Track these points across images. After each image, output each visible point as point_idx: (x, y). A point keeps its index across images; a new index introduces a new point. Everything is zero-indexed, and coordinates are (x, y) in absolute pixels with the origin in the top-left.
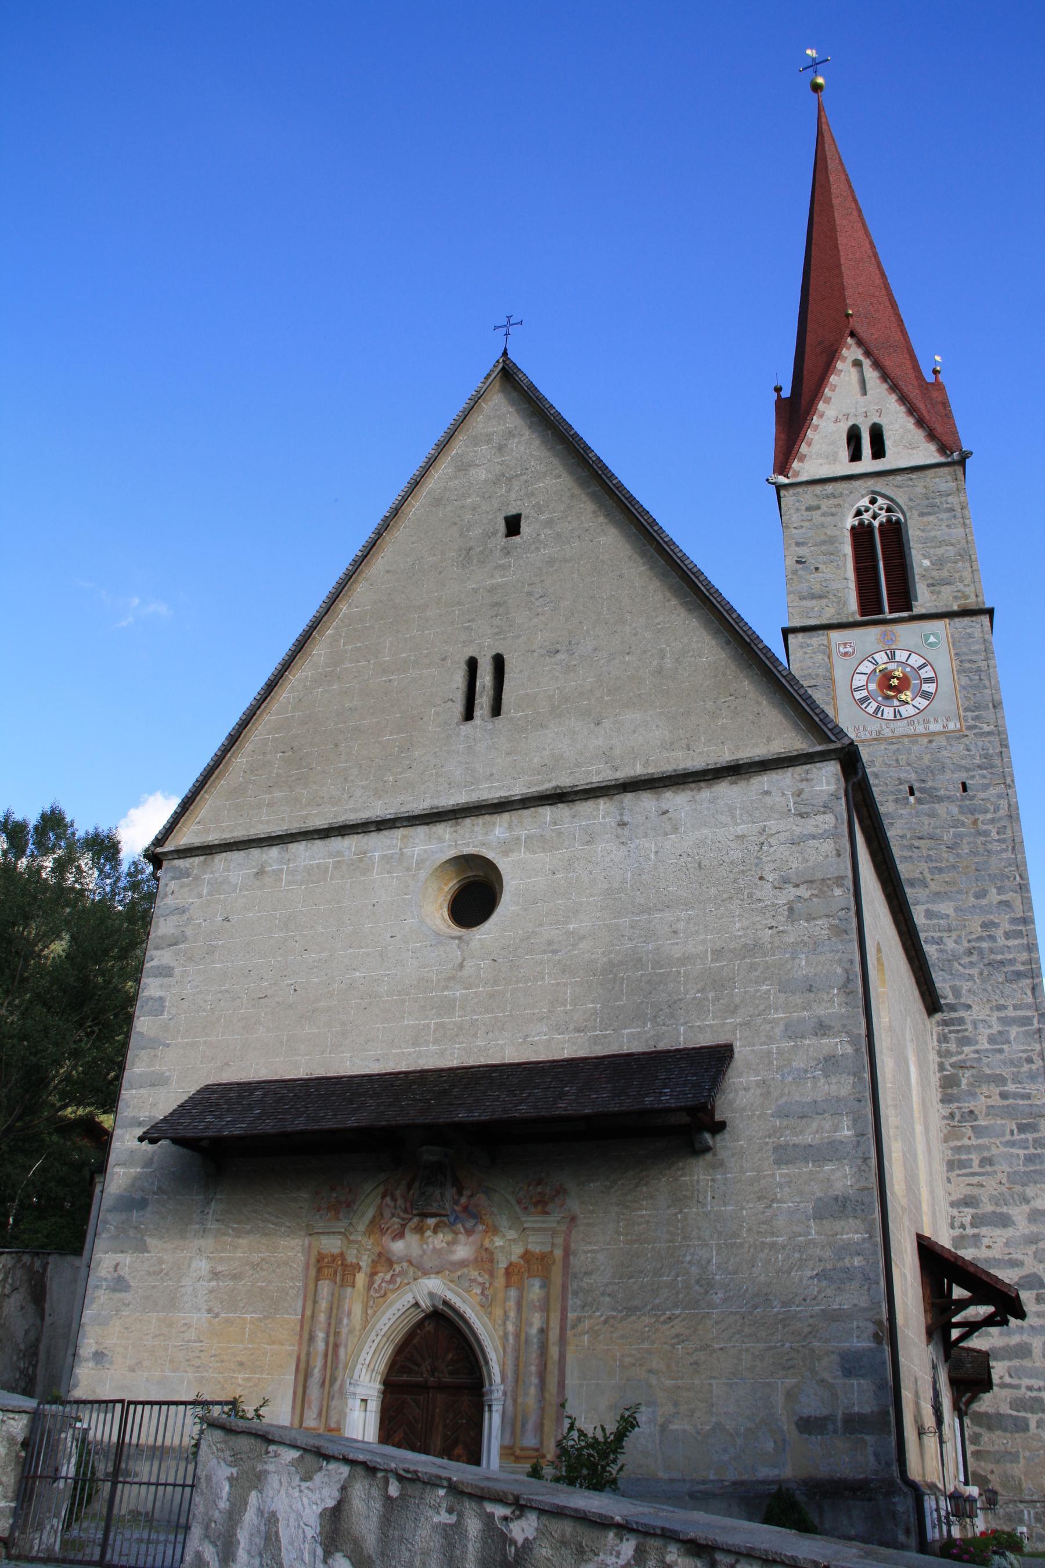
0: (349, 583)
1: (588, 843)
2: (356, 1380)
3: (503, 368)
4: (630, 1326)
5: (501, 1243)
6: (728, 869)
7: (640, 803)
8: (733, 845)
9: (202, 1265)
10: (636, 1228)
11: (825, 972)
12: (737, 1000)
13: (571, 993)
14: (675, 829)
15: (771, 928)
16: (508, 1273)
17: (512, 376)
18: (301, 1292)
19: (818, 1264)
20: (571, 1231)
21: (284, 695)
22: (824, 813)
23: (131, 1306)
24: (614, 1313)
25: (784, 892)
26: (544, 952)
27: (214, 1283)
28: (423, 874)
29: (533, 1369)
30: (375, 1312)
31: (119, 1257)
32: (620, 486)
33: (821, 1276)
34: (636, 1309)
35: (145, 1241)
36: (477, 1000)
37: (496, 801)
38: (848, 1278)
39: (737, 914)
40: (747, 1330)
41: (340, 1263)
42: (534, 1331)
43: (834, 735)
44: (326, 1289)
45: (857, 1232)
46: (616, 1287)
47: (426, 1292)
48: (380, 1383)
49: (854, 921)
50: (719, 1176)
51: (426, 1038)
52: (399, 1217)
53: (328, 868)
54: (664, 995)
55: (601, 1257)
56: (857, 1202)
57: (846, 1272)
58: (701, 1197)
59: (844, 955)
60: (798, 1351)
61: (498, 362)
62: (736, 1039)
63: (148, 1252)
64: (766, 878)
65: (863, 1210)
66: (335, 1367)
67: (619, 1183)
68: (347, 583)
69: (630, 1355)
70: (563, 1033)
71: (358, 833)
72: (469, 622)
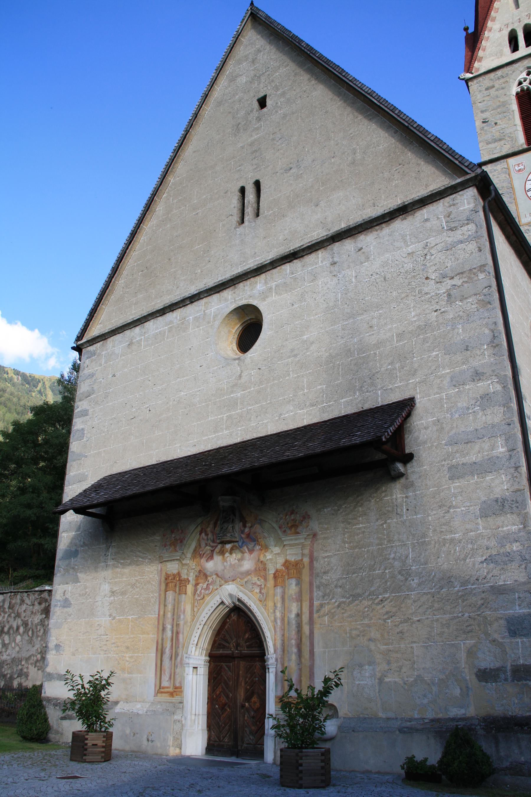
0: (173, 164)
1: (313, 281)
2: (190, 655)
3: (251, 13)
4: (355, 608)
5: (271, 557)
6: (404, 277)
7: (344, 247)
8: (406, 260)
9: (106, 588)
10: (356, 537)
11: (476, 334)
12: (416, 366)
13: (307, 381)
14: (367, 258)
15: (436, 311)
16: (275, 577)
17: (256, 15)
18: (158, 600)
19: (486, 551)
20: (313, 544)
21: (142, 238)
22: (468, 224)
23: (72, 616)
24: (344, 600)
25: (443, 284)
26: (289, 357)
27: (112, 598)
28: (217, 323)
29: (293, 642)
30: (199, 609)
31: (65, 587)
32: (321, 57)
33: (490, 560)
34: (359, 595)
35: (77, 576)
36: (250, 397)
37: (255, 267)
38: (509, 560)
39: (412, 306)
40: (436, 605)
41: (178, 579)
42: (293, 616)
43: (470, 169)
44: (171, 597)
45: (514, 524)
46: (344, 581)
47: (227, 594)
48: (205, 655)
49: (496, 296)
50: (411, 494)
51: (221, 426)
52: (210, 546)
53: (165, 332)
54: (366, 371)
55: (333, 560)
56: (513, 501)
57: (507, 556)
58: (399, 510)
59: (490, 319)
60: (474, 619)
61: (248, 10)
62: (417, 393)
63: (80, 582)
64: (431, 277)
65: (517, 507)
66: (177, 647)
67: (343, 506)
68: (171, 164)
69: (356, 629)
70: (303, 409)
71: (181, 307)
72: (240, 166)
